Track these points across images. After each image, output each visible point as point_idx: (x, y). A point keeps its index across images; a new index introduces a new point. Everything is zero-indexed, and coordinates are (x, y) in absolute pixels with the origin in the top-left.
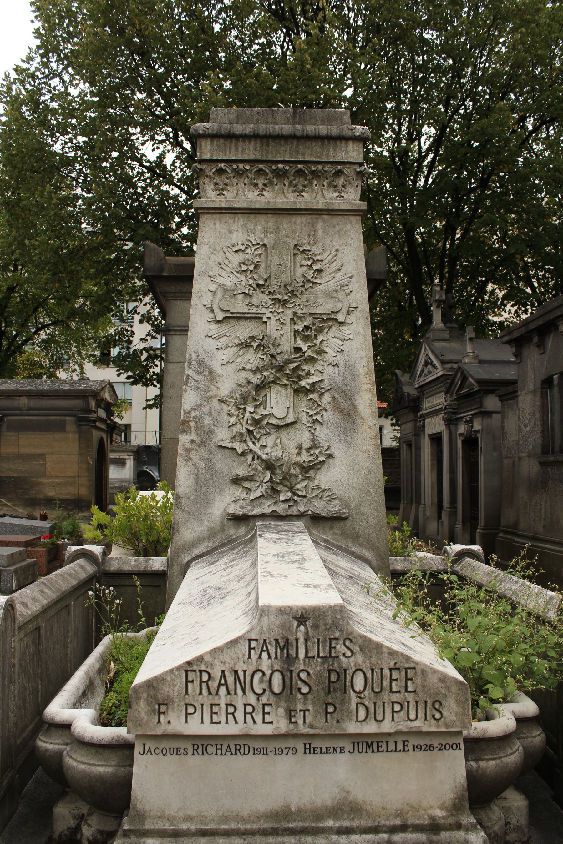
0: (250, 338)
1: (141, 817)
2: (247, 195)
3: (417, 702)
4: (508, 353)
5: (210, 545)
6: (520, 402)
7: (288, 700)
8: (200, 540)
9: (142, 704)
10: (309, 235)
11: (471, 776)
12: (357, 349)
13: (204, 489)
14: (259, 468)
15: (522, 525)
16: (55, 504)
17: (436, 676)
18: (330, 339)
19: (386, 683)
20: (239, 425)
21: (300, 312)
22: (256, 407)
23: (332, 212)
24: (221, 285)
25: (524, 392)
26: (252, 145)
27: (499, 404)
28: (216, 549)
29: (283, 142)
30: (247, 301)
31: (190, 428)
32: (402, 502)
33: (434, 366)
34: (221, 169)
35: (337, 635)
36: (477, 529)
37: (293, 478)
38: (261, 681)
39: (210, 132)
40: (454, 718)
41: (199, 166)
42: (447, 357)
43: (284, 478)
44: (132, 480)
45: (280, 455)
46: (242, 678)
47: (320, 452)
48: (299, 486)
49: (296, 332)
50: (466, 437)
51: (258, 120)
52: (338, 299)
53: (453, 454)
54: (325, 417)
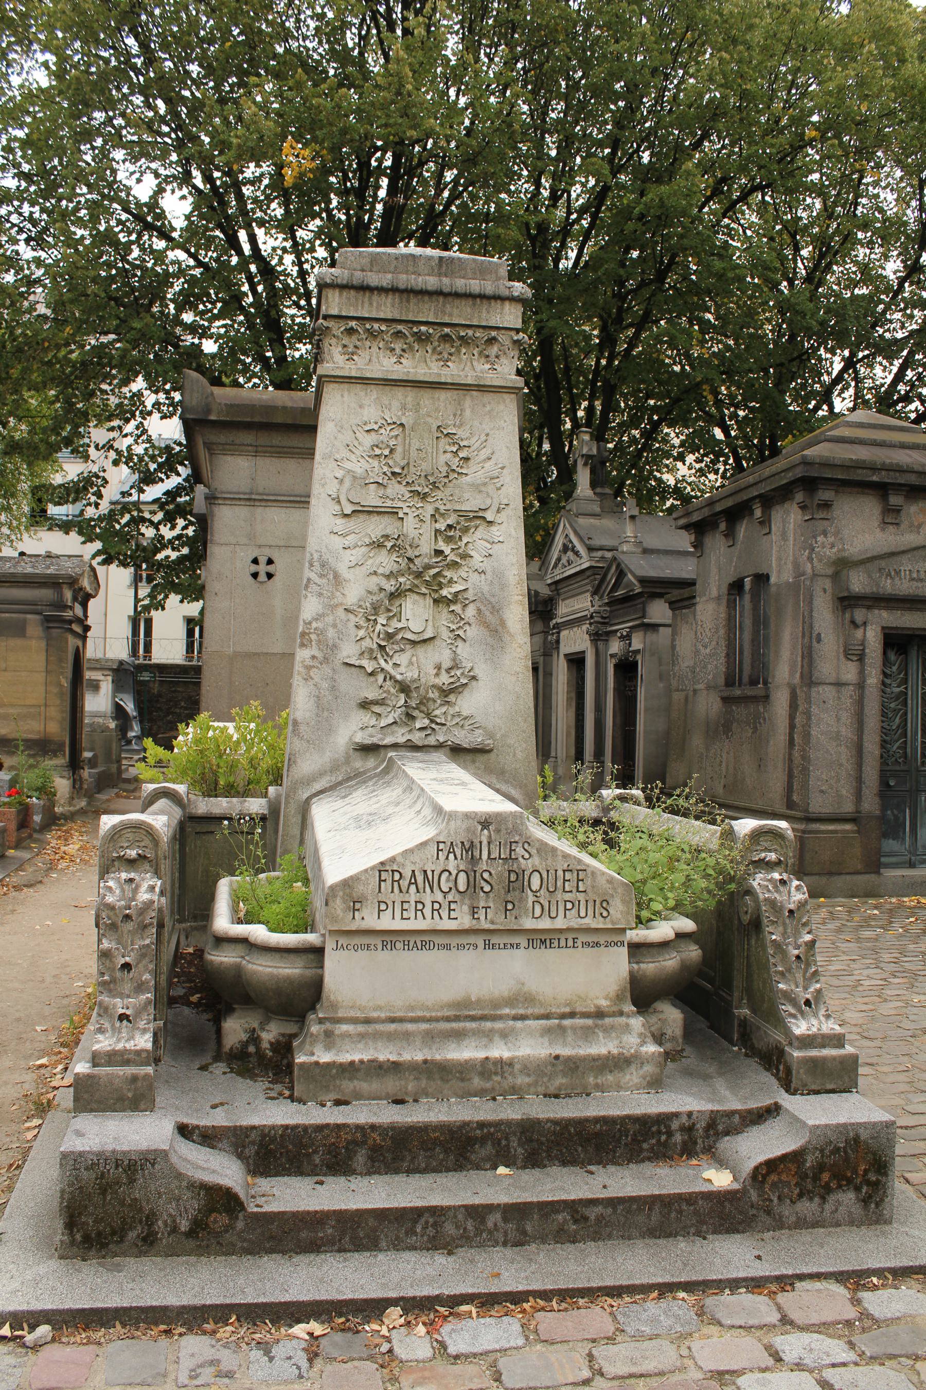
0: (383, 536)
1: (334, 1006)
2: (380, 362)
4: (684, 541)
5: (333, 779)
6: (698, 613)
7: (471, 898)
8: (321, 774)
9: (338, 901)
10: (455, 415)
11: (631, 973)
12: (507, 554)
13: (326, 713)
14: (392, 690)
16: (17, 747)
17: (604, 878)
18: (477, 542)
20: (368, 640)
21: (442, 508)
22: (389, 619)
23: (482, 388)
24: (349, 471)
25: (704, 599)
26: (389, 300)
27: (669, 613)
28: (340, 783)
29: (426, 298)
30: (381, 493)
31: (311, 641)
33: (577, 553)
34: (352, 328)
35: (517, 838)
37: (431, 702)
38: (448, 880)
39: (339, 281)
40: (620, 916)
41: (325, 324)
42: (596, 542)
43: (421, 703)
44: (109, 714)
45: (416, 676)
47: (463, 674)
48: (437, 712)
49: (437, 531)
50: (620, 660)
51: (396, 267)
52: (488, 494)
53: (600, 682)
54: (468, 633)
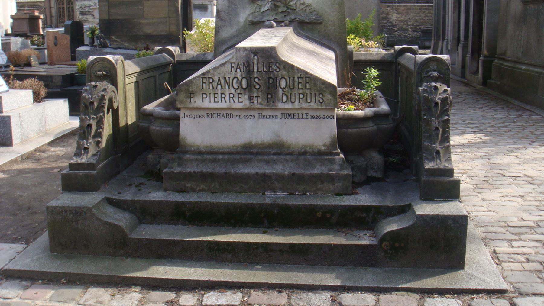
3: (311, 94)
15: (509, 53)
19: (296, 84)
32: (433, 38)
35: (272, 61)
36: (480, 57)
38: (237, 83)
46: (228, 81)
